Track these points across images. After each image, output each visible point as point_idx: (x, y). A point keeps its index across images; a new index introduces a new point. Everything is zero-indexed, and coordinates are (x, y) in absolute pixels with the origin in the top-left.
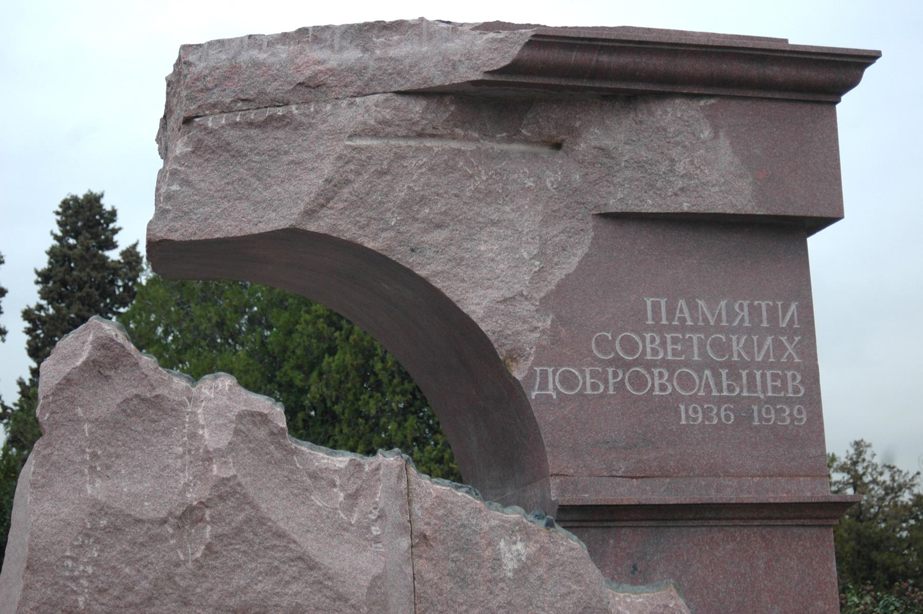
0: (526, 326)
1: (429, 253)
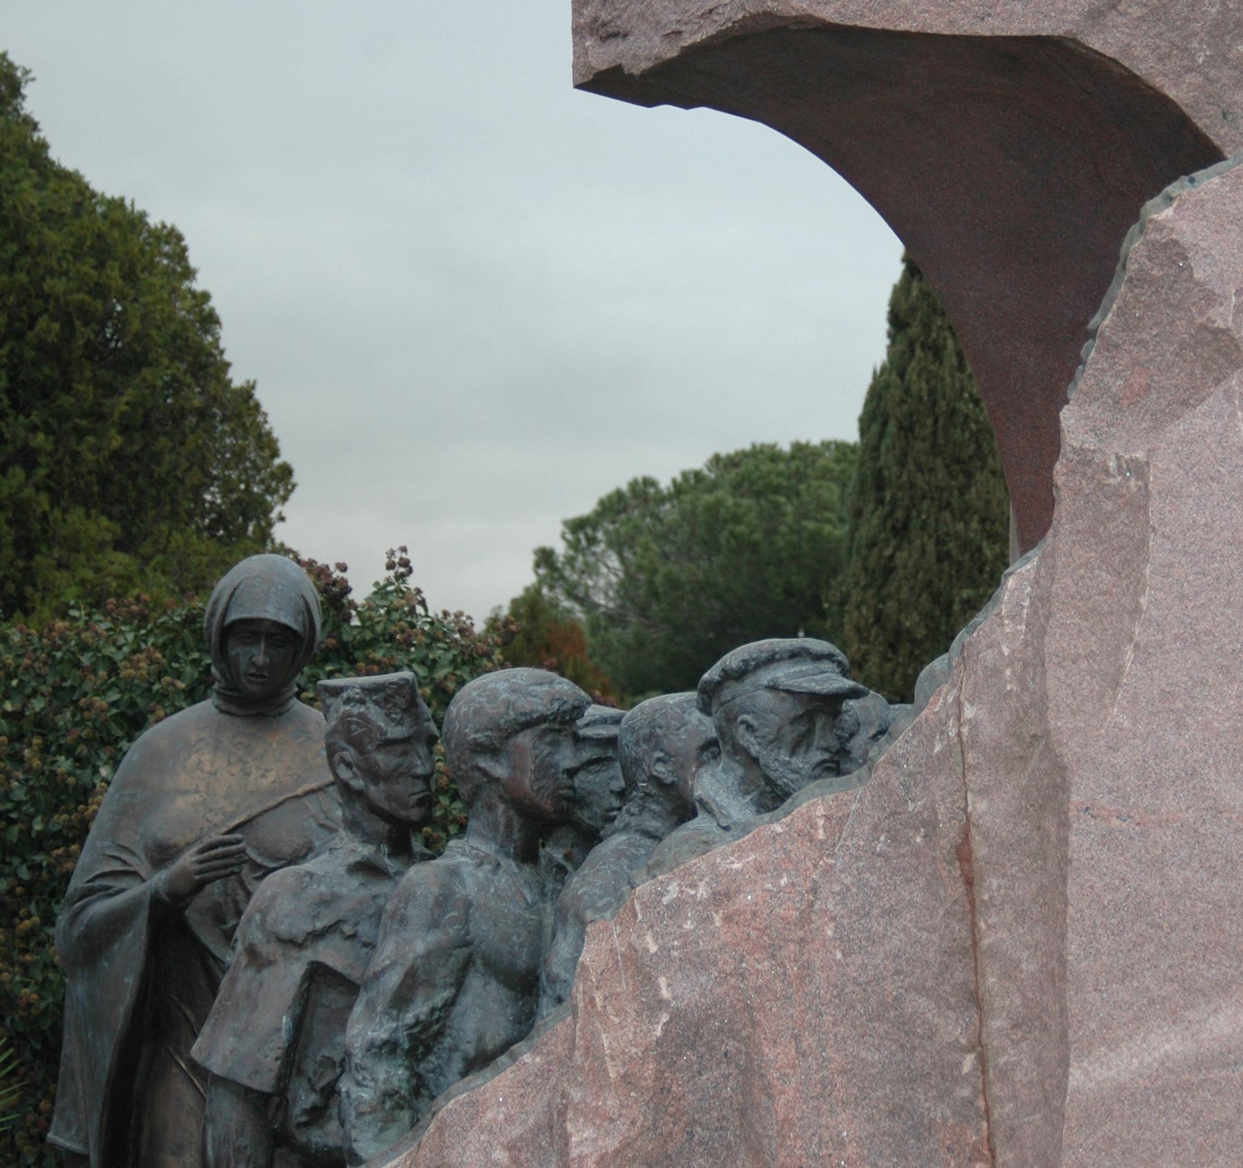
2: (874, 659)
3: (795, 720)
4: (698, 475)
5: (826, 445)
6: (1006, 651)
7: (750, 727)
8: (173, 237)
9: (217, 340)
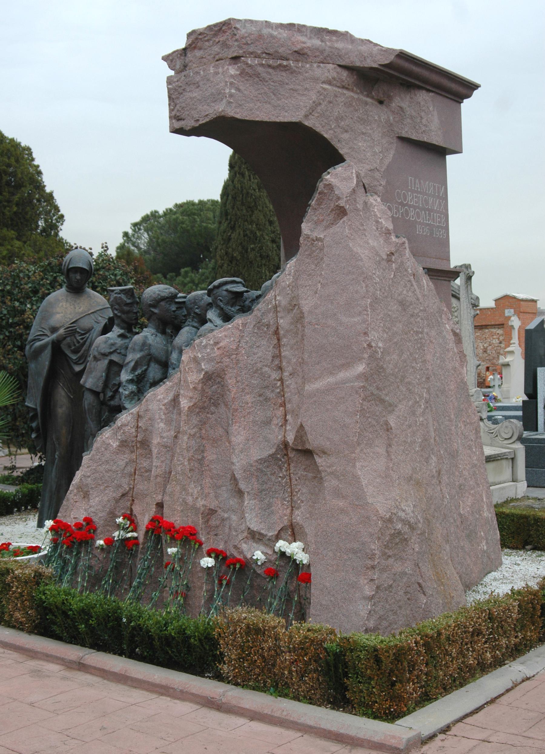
0: (378, 183)
1: (343, 143)
2: (226, 265)
3: (232, 298)
4: (171, 210)
5: (208, 201)
6: (288, 283)
7: (221, 301)
8: (29, 149)
9: (42, 178)
